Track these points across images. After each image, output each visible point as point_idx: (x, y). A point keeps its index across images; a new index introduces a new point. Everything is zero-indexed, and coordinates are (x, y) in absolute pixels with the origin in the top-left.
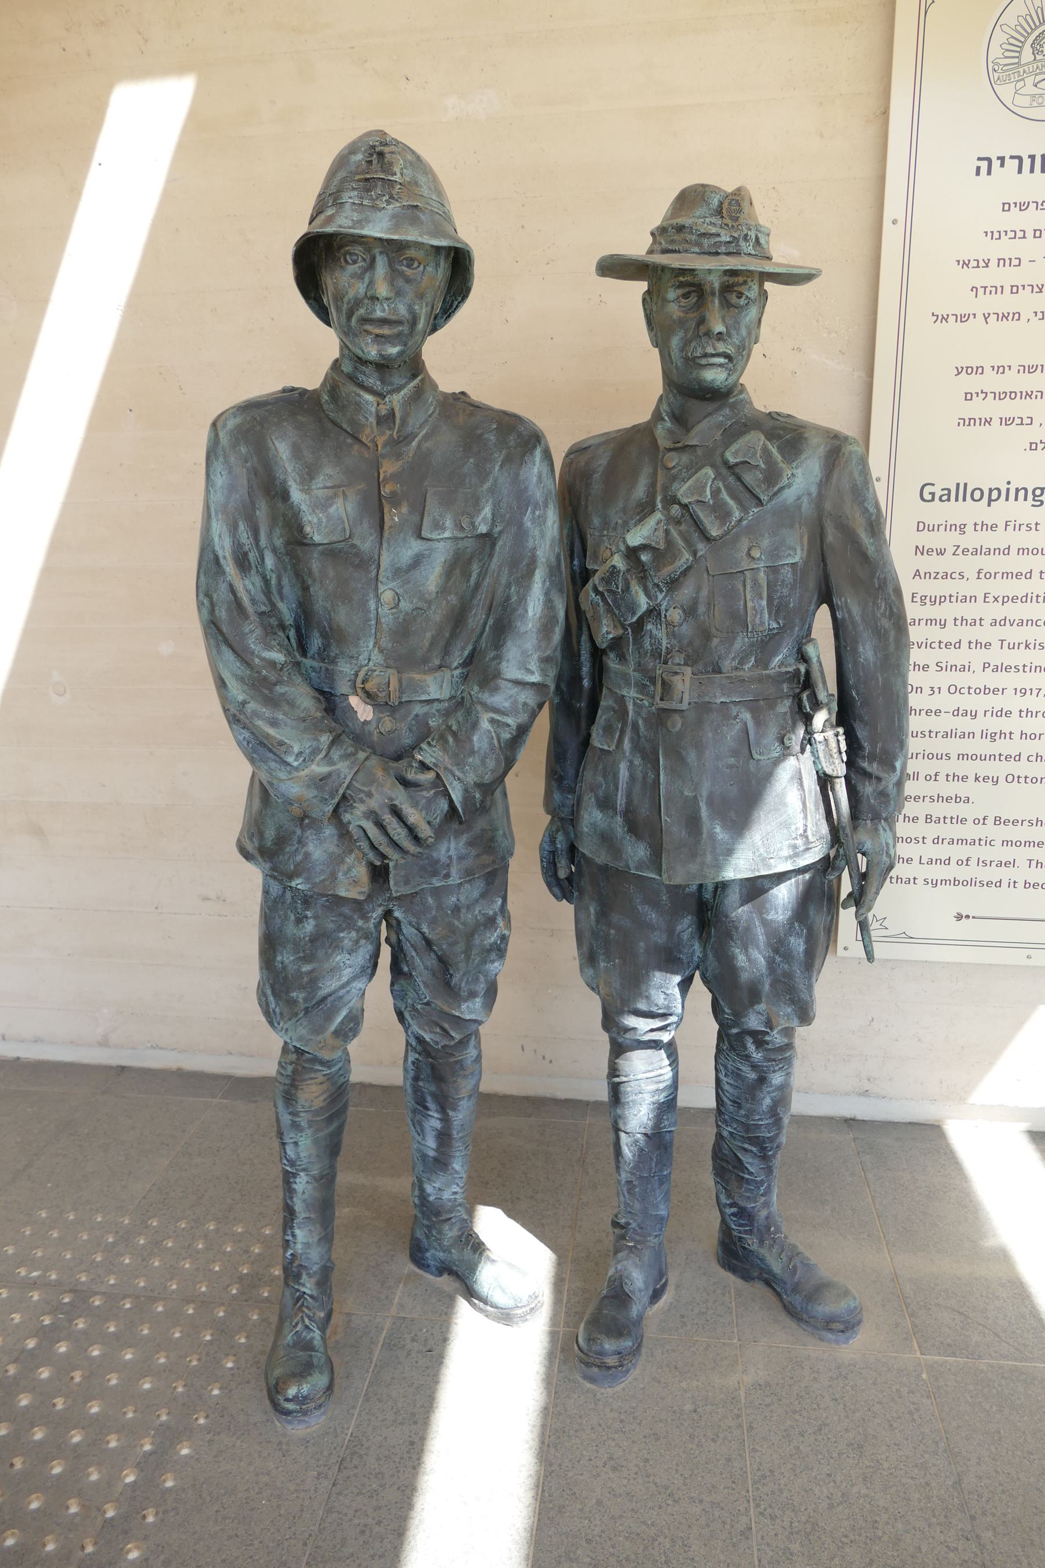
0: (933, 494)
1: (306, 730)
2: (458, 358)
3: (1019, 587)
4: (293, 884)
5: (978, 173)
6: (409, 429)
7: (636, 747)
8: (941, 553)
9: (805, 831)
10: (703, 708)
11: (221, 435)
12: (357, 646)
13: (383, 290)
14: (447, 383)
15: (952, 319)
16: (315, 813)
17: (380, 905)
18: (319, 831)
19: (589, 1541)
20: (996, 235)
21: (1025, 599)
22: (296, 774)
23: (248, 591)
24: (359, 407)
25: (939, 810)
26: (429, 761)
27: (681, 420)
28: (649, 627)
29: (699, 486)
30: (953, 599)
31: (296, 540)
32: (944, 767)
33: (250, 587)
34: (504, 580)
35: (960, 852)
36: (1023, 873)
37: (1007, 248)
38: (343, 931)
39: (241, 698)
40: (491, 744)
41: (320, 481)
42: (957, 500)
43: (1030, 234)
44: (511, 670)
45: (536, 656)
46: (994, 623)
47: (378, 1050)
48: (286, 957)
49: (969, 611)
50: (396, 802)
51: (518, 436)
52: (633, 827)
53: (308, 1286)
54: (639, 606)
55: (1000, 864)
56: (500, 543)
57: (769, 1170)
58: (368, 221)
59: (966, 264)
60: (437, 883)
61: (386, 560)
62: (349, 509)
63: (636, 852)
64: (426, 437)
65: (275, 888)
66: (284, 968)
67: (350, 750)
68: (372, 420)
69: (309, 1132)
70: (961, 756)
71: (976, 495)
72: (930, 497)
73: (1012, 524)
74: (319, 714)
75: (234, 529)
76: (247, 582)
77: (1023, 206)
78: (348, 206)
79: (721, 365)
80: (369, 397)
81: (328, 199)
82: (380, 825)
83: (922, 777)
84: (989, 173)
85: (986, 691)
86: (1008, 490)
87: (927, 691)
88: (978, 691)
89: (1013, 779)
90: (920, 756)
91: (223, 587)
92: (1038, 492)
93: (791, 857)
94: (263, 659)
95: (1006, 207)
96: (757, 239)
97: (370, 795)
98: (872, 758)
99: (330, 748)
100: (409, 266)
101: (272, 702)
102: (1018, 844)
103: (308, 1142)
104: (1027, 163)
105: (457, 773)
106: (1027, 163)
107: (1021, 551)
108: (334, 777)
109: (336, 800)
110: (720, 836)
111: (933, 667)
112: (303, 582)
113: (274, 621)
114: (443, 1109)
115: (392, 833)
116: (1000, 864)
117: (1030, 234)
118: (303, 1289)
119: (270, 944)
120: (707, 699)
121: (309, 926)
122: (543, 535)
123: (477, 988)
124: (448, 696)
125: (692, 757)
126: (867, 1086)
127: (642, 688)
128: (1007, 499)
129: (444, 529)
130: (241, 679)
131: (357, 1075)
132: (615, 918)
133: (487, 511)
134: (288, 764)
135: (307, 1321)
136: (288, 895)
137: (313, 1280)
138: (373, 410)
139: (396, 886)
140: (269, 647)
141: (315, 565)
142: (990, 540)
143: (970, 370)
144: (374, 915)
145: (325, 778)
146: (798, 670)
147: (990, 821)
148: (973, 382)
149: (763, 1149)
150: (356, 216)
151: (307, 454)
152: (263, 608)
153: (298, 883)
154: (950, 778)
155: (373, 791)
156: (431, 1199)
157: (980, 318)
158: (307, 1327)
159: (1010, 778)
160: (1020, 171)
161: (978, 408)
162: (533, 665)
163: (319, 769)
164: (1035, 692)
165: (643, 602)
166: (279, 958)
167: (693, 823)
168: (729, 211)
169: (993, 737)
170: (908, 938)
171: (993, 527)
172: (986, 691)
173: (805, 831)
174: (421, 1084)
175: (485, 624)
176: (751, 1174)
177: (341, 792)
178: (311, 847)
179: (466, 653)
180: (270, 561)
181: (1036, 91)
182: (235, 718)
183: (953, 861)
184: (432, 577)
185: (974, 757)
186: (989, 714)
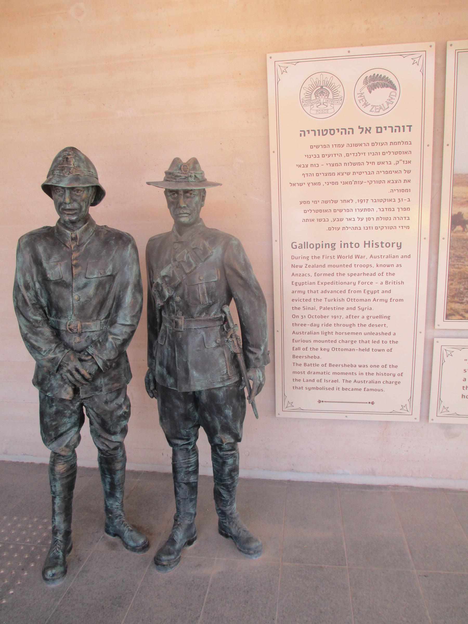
0: (296, 246)
1: (47, 343)
2: (100, 214)
3: (330, 279)
4: (48, 394)
5: (301, 135)
6: (82, 241)
7: (169, 344)
8: (301, 267)
9: (227, 372)
11: (21, 244)
12: (67, 313)
13: (68, 200)
15: (297, 185)
16: (52, 371)
17: (78, 401)
18: (55, 376)
19: (143, 620)
20: (309, 156)
21: (332, 283)
22: (44, 358)
23: (28, 297)
24: (65, 235)
25: (309, 361)
26: (90, 352)
27: (180, 233)
28: (171, 303)
30: (307, 283)
31: (45, 281)
32: (309, 345)
33: (29, 295)
34: (118, 290)
36: (341, 385)
37: (313, 161)
38: (66, 410)
39: (26, 332)
40: (113, 346)
41: (53, 259)
42: (305, 248)
43: (321, 156)
44: (120, 320)
45: (129, 316)
46: (322, 292)
47: (87, 454)
48: (47, 420)
49: (313, 288)
50: (77, 367)
52: (169, 372)
53: (59, 537)
54: (166, 296)
55: (333, 381)
56: (117, 277)
57: (231, 496)
58: (61, 181)
59: (300, 166)
61: (74, 285)
62: (62, 269)
63: (170, 381)
64: (89, 243)
66: (47, 423)
67: (63, 349)
68: (70, 239)
69: (59, 482)
70: (315, 341)
72: (295, 247)
73: (325, 256)
74: (52, 338)
75: (24, 276)
76: (28, 293)
77: (317, 147)
78: (56, 175)
79: (186, 216)
80: (68, 232)
82: (72, 374)
83: (301, 349)
84: (305, 136)
85: (322, 317)
86: (322, 244)
87: (300, 317)
88: (319, 317)
89: (334, 349)
90: (300, 341)
91: (20, 295)
92: (333, 245)
93: (221, 382)
94: (33, 319)
95: (312, 147)
96: (195, 176)
97: (68, 364)
98: (253, 346)
99: (55, 349)
100: (77, 192)
101: (36, 334)
102: (338, 374)
103: (59, 485)
104: (317, 133)
105: (100, 356)
106: (317, 133)
107: (329, 266)
108: (56, 359)
109: (57, 366)
110: (195, 375)
111: (302, 308)
112: (48, 292)
113: (37, 306)
114: (111, 474)
115: (76, 377)
116: (333, 381)
117: (321, 156)
118: (58, 538)
119: (42, 414)
120: (189, 327)
121: (54, 409)
122: (131, 275)
123: (117, 430)
124: (99, 329)
125: (185, 347)
127: (170, 324)
128: (322, 248)
129: (94, 274)
130: (26, 326)
131: (80, 463)
132: (167, 404)
133: (110, 267)
134: (42, 354)
135: (58, 549)
136: (47, 398)
137: (61, 535)
138: (70, 236)
139: (82, 395)
140: (35, 315)
143: (305, 202)
144: (77, 405)
145: (53, 359)
146: (222, 317)
147: (328, 365)
148: (307, 207)
149: (228, 488)
150: (58, 179)
151: (49, 251)
152: (34, 302)
153: (49, 394)
154: (391, 342)
155: (69, 363)
156: (109, 508)
157: (306, 184)
158: (57, 551)
159: (333, 349)
160: (315, 135)
162: (128, 318)
163: (51, 356)
164: (339, 317)
166: (45, 420)
167: (187, 371)
168: (184, 169)
169: (326, 334)
170: (301, 410)
171: (319, 257)
172: (322, 317)
173: (227, 372)
174: (103, 465)
175: (113, 304)
176: (224, 497)
177: (59, 363)
178: (53, 382)
179: (106, 314)
180: (37, 285)
181: (317, 109)
182: (25, 339)
183: (316, 381)
184: (91, 290)
185: (320, 341)
186: (323, 325)
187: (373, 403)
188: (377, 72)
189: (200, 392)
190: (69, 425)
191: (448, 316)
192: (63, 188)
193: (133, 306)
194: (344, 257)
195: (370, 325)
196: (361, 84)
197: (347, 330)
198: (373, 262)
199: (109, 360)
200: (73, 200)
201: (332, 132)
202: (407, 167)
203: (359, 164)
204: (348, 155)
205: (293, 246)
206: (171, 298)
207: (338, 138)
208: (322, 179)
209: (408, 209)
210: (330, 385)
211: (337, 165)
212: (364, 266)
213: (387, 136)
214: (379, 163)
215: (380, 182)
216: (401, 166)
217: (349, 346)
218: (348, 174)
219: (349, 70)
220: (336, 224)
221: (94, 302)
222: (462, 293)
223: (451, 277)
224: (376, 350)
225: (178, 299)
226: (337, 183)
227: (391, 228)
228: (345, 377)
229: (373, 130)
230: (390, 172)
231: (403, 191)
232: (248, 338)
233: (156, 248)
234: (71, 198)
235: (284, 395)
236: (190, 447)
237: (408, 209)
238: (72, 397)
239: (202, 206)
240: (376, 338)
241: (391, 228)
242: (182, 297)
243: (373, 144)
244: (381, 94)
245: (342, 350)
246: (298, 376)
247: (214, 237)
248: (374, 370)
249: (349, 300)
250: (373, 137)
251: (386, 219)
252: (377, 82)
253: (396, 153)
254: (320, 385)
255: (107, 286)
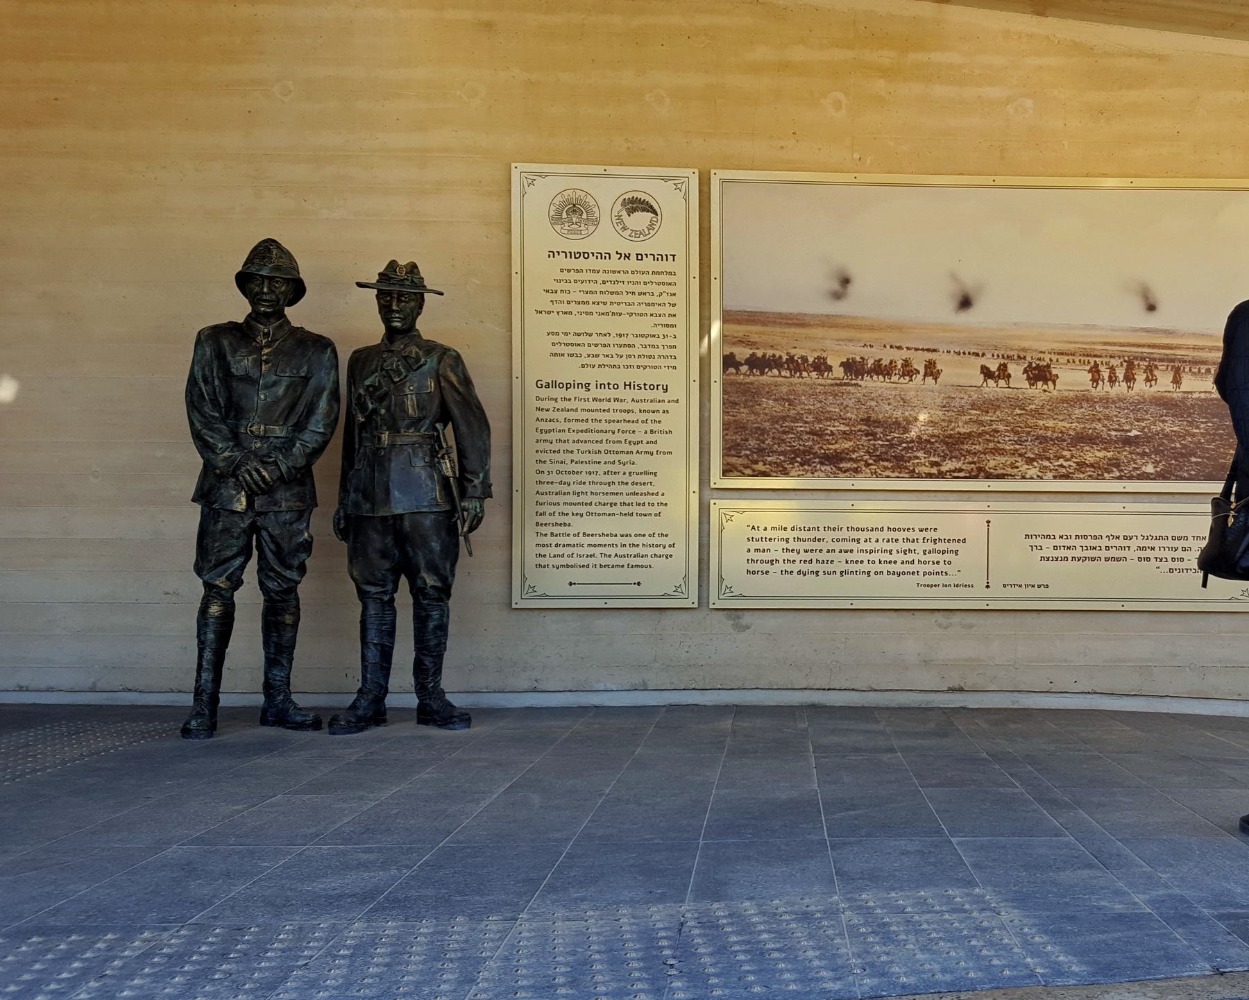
2: (296, 315)
3: (583, 426)
10: (392, 445)
14: (295, 324)
21: (586, 431)
25: (557, 530)
29: (393, 362)
35: (568, 551)
44: (312, 427)
51: (323, 344)
60: (276, 509)
65: (207, 510)
71: (561, 386)
81: (249, 261)
89: (589, 514)
95: (562, 271)
102: (595, 546)
126: (535, 684)
133: (305, 368)
141: (234, 384)
142: (568, 405)
143: (553, 333)
148: (555, 339)
161: (557, 349)
165: (370, 406)
167: (387, 492)
180: (216, 382)
185: (571, 504)
187: (639, 584)
188: (636, 195)
189: (401, 516)
190: (235, 549)
191: (727, 471)
192: (262, 276)
193: (328, 415)
194: (600, 400)
195: (633, 483)
196: (618, 206)
197: (606, 489)
198: (636, 407)
199: (295, 468)
200: (271, 291)
201: (586, 255)
202: (672, 300)
203: (617, 293)
204: (604, 282)
205: (539, 384)
206: (375, 411)
207: (592, 263)
208: (573, 308)
209: (675, 347)
210: (584, 561)
211: (591, 292)
212: (625, 411)
213: (648, 264)
214: (640, 294)
215: (641, 315)
216: (665, 299)
217: (607, 509)
218: (605, 303)
219: (606, 192)
220: (591, 361)
221: (283, 404)
222: (739, 445)
223: (726, 426)
224: (641, 515)
225: (383, 411)
226: (591, 313)
227: (655, 367)
228: (603, 550)
229: (633, 257)
230: (653, 304)
231: (668, 326)
232: (465, 462)
233: (361, 359)
234: (269, 288)
235: (524, 578)
236: (386, 598)
237: (675, 347)
238: (240, 532)
239: (419, 314)
240: (641, 499)
241: (655, 367)
242: (388, 409)
243: (633, 272)
244: (641, 220)
245: (599, 515)
246: (543, 551)
247: (431, 348)
248: (640, 541)
249: (607, 452)
250: (633, 264)
251: (650, 357)
252: (637, 205)
253: (659, 284)
254: (571, 561)
255: (299, 389)
